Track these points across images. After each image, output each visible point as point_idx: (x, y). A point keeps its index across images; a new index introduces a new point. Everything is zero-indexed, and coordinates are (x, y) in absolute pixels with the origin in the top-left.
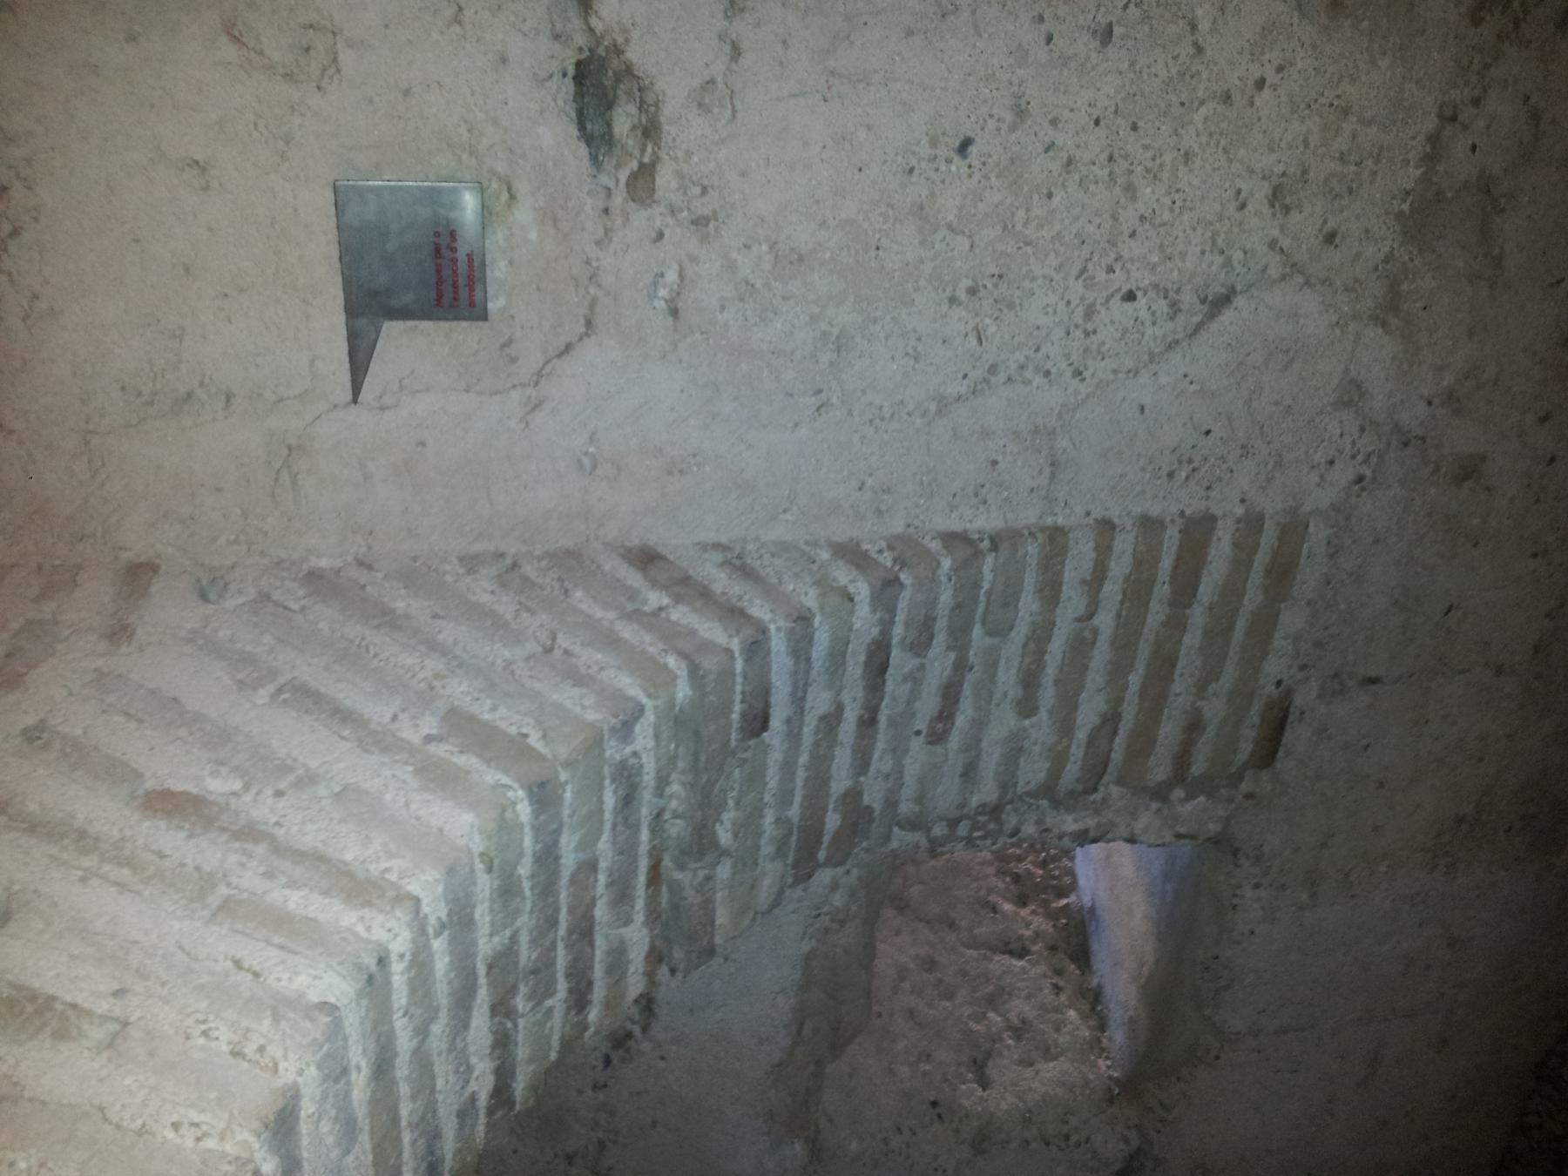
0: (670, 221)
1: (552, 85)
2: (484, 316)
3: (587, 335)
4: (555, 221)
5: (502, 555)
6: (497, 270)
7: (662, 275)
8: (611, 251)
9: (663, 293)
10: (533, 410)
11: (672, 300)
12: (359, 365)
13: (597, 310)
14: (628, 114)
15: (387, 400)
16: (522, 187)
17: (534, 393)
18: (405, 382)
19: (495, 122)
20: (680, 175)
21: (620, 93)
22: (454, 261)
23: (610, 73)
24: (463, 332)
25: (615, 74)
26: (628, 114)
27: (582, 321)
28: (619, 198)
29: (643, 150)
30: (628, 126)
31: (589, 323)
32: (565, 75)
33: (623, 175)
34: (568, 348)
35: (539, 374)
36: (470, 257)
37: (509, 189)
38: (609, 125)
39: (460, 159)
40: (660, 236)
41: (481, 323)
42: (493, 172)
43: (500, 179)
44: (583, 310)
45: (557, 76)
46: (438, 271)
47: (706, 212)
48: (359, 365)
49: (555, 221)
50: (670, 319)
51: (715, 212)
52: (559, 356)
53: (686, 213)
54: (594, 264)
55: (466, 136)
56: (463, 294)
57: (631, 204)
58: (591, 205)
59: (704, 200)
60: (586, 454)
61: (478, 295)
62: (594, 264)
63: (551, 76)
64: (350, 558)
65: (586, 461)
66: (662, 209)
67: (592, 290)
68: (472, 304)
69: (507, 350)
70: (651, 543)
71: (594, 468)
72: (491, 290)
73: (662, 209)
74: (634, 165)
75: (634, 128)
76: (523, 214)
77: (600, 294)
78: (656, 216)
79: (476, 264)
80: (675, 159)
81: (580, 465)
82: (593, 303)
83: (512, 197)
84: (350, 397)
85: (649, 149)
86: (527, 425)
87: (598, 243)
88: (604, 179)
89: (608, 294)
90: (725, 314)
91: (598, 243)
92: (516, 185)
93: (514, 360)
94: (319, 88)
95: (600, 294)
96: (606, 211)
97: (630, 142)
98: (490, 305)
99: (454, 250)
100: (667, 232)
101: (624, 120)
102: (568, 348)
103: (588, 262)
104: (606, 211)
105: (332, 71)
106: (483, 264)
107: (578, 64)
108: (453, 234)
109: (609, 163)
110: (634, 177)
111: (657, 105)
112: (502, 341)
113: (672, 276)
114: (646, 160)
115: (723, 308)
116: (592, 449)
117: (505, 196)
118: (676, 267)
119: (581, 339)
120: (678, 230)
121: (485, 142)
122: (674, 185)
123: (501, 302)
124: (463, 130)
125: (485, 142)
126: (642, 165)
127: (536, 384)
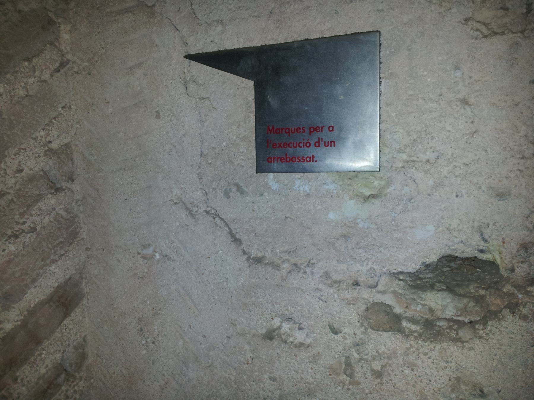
0: (349, 341)
1: (476, 240)
2: (261, 169)
3: (248, 259)
4: (346, 236)
5: (71, 179)
6: (299, 183)
7: (300, 329)
8: (321, 286)
9: (286, 327)
10: (187, 209)
11: (279, 335)
12: (225, 60)
13: (269, 269)
14: (444, 307)
15: (192, 87)
16: (375, 208)
17: (201, 210)
18: (207, 102)
19: (437, 186)
20: (392, 355)
21: (466, 301)
22: (307, 145)
23: (482, 292)
24: (248, 152)
25: (482, 297)
26: (444, 307)
27: (260, 255)
28: (366, 294)
29: (412, 320)
30: (433, 305)
31: (258, 260)
32: (482, 251)
33: (388, 299)
34: (237, 241)
35: (216, 215)
36: (312, 159)
37: (373, 196)
38: (432, 287)
39: (400, 151)
40: (335, 332)
41: (255, 168)
42: (389, 183)
43: (383, 188)
44: (268, 255)
45: (482, 245)
46: (298, 130)
47: (358, 375)
48: (225, 60)
49: (346, 236)
50: (264, 331)
51: (358, 383)
52: (231, 233)
53: (356, 356)
54: (308, 270)
55: (423, 157)
56: (277, 152)
57: (364, 307)
58: (361, 270)
59: (369, 374)
60: (154, 251)
61: (277, 165)
62: (308, 270)
63: (485, 240)
64: (69, 57)
65: (150, 251)
66: (360, 336)
67: (286, 265)
68: (270, 160)
69: (234, 189)
70: (84, 302)
71: (144, 257)
72: (283, 176)
73: (360, 336)
74: (398, 310)
75: (432, 311)
76: (351, 208)
77: (284, 272)
78: (353, 330)
79: (305, 164)
80: (406, 353)
81: (145, 247)
82: (276, 267)
83: (367, 199)
84: (193, 51)
85: (414, 327)
86: (176, 203)
87: (327, 274)
88: (384, 280)
89: (283, 280)
90: (268, 381)
91: (327, 274)
92: (377, 202)
93: (227, 194)
94: (467, 20)
95: (284, 272)
96: (356, 284)
97: (419, 307)
98: (271, 176)
99: (317, 144)
100: (338, 337)
101: (441, 303)
102: (237, 241)
103: (309, 264)
104: (356, 284)
105: (484, 29)
106: (305, 171)
107: (493, 264)
108: (332, 143)
109: (398, 286)
110: (387, 309)
111: (457, 340)
112: (242, 184)
113: (300, 337)
114: (404, 324)
115: (273, 379)
116: (158, 256)
117: (367, 192)
118: (308, 341)
119: (244, 253)
120: (341, 348)
121: (418, 176)
122: (382, 349)
123: (275, 186)
124: (430, 155)
125: (418, 176)
126: (398, 318)
127: (207, 212)
